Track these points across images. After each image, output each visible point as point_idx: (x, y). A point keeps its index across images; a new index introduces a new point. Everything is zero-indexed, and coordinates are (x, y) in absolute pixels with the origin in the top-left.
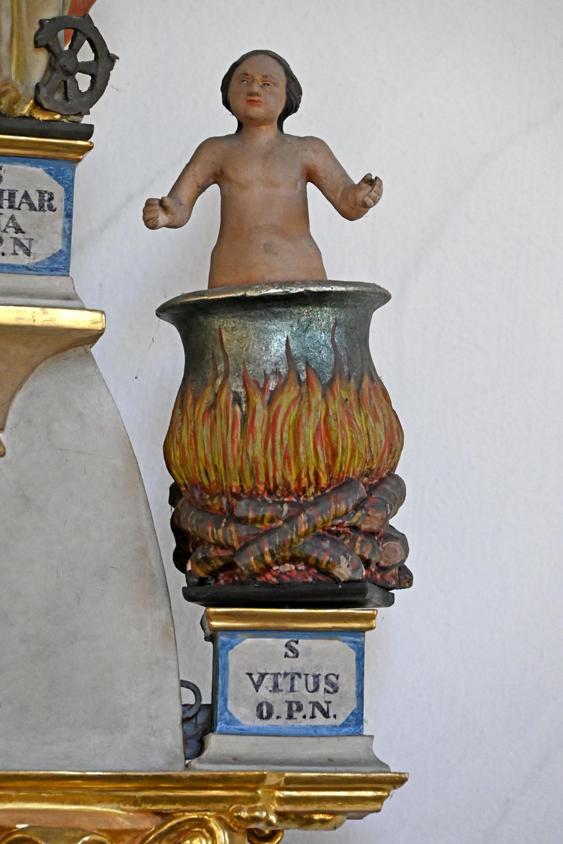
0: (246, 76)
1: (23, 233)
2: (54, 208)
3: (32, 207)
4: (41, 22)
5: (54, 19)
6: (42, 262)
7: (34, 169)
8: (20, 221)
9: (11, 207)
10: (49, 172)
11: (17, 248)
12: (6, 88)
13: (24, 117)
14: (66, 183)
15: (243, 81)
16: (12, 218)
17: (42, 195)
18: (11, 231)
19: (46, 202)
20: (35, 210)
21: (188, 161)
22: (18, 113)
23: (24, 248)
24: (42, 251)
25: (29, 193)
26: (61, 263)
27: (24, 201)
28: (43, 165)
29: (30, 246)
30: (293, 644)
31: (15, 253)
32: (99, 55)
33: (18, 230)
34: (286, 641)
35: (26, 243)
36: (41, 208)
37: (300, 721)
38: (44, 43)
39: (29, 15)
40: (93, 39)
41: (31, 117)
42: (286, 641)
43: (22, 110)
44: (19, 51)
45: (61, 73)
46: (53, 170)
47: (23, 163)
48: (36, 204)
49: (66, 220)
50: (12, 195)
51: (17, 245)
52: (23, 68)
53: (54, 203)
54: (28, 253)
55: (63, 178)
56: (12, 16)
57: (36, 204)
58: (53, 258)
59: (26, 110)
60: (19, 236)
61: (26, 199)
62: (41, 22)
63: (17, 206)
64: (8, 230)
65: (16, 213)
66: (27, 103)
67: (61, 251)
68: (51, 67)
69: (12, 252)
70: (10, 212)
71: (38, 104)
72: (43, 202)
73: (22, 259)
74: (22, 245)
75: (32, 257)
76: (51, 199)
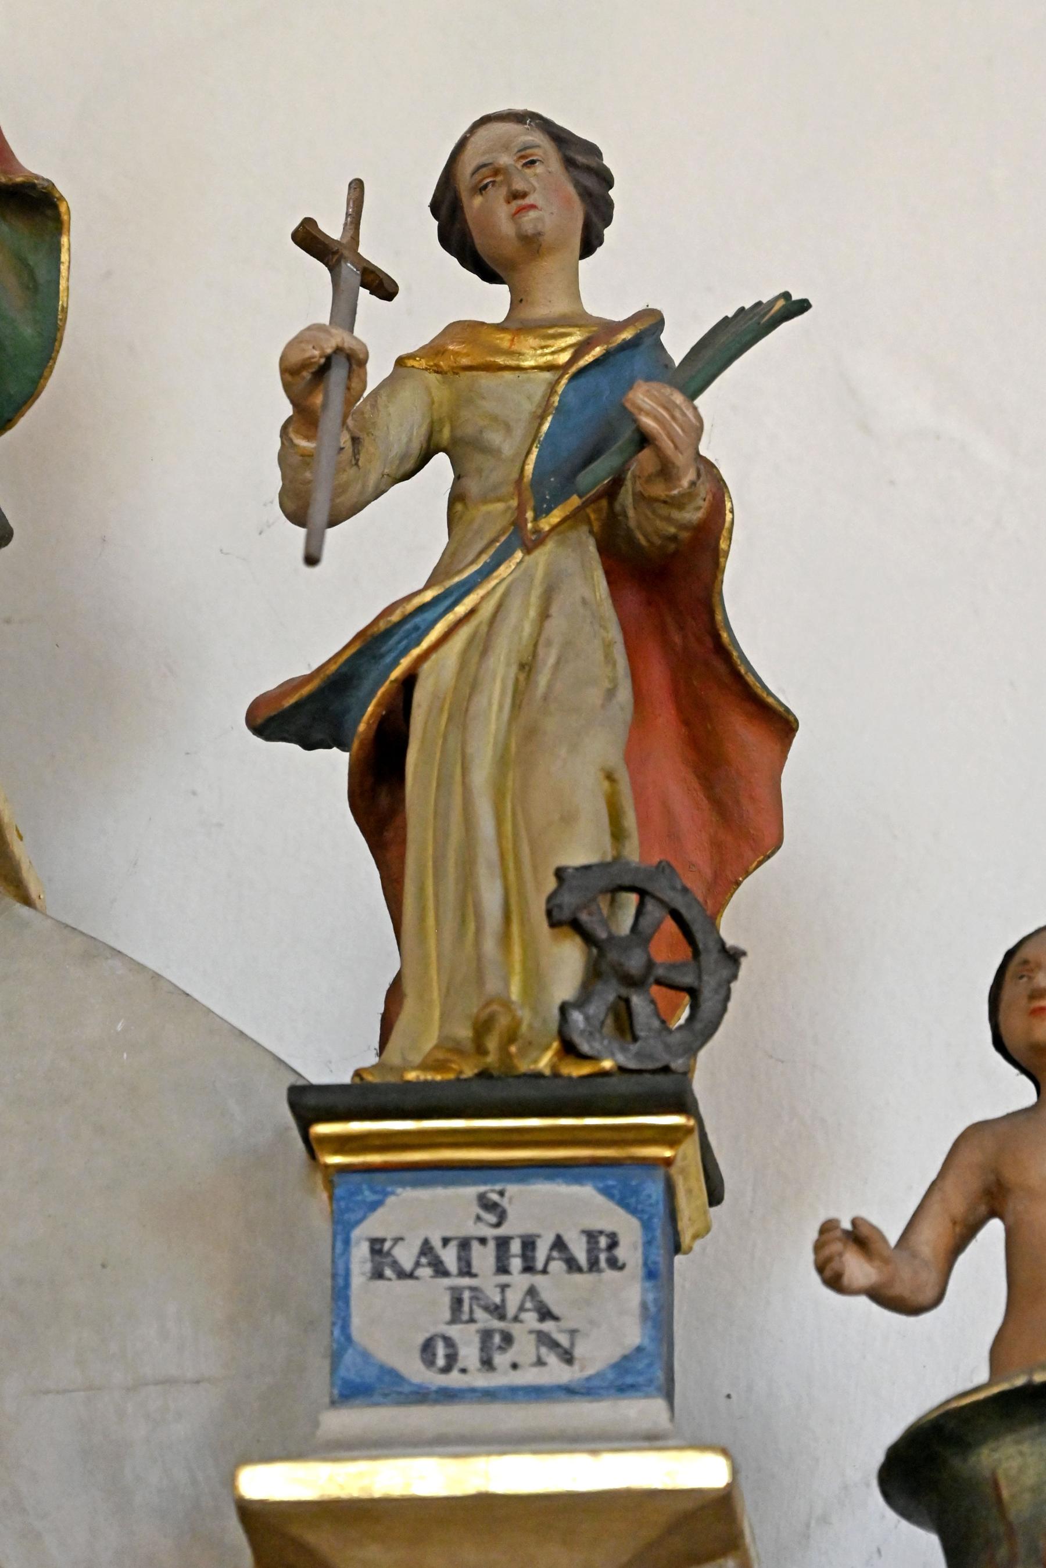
0: (1027, 967)
1: (556, 1318)
2: (620, 1264)
3: (572, 1266)
4: (560, 874)
5: (587, 868)
6: (600, 1375)
7: (575, 1189)
8: (549, 1296)
9: (528, 1269)
10: (607, 1192)
11: (544, 1350)
12: (488, 1011)
13: (538, 1076)
14: (643, 1211)
15: (1022, 977)
16: (532, 1292)
17: (592, 1240)
18: (530, 1318)
19: (603, 1251)
20: (580, 1270)
21: (933, 1175)
22: (524, 1066)
23: (560, 1350)
24: (596, 1354)
25: (566, 1238)
26: (640, 1373)
27: (555, 1254)
28: (593, 1178)
29: (572, 1344)
31: (540, 1362)
32: (701, 946)
33: (545, 1314)
35: (563, 1340)
36: (594, 1265)
38: (566, 915)
39: (535, 868)
40: (683, 911)
41: (556, 1075)
43: (536, 1061)
44: (525, 947)
45: (614, 982)
46: (613, 1187)
47: (550, 1178)
48: (582, 1258)
49: (648, 1284)
50: (529, 1244)
51: (544, 1344)
52: (535, 979)
53: (620, 1253)
54: (568, 1357)
55: (638, 1202)
56: (505, 877)
57: (582, 1258)
58: (624, 1365)
59: (544, 1062)
60: (548, 1326)
61: (560, 1251)
62: (560, 874)
63: (540, 1265)
64: (524, 1316)
65: (539, 1280)
66: (547, 1048)
67: (639, 1349)
68: (594, 974)
69: (534, 1359)
70: (527, 1280)
71: (569, 1049)
72: (595, 1252)
73: (556, 1372)
74: (554, 1345)
75: (576, 1367)
76: (613, 1245)
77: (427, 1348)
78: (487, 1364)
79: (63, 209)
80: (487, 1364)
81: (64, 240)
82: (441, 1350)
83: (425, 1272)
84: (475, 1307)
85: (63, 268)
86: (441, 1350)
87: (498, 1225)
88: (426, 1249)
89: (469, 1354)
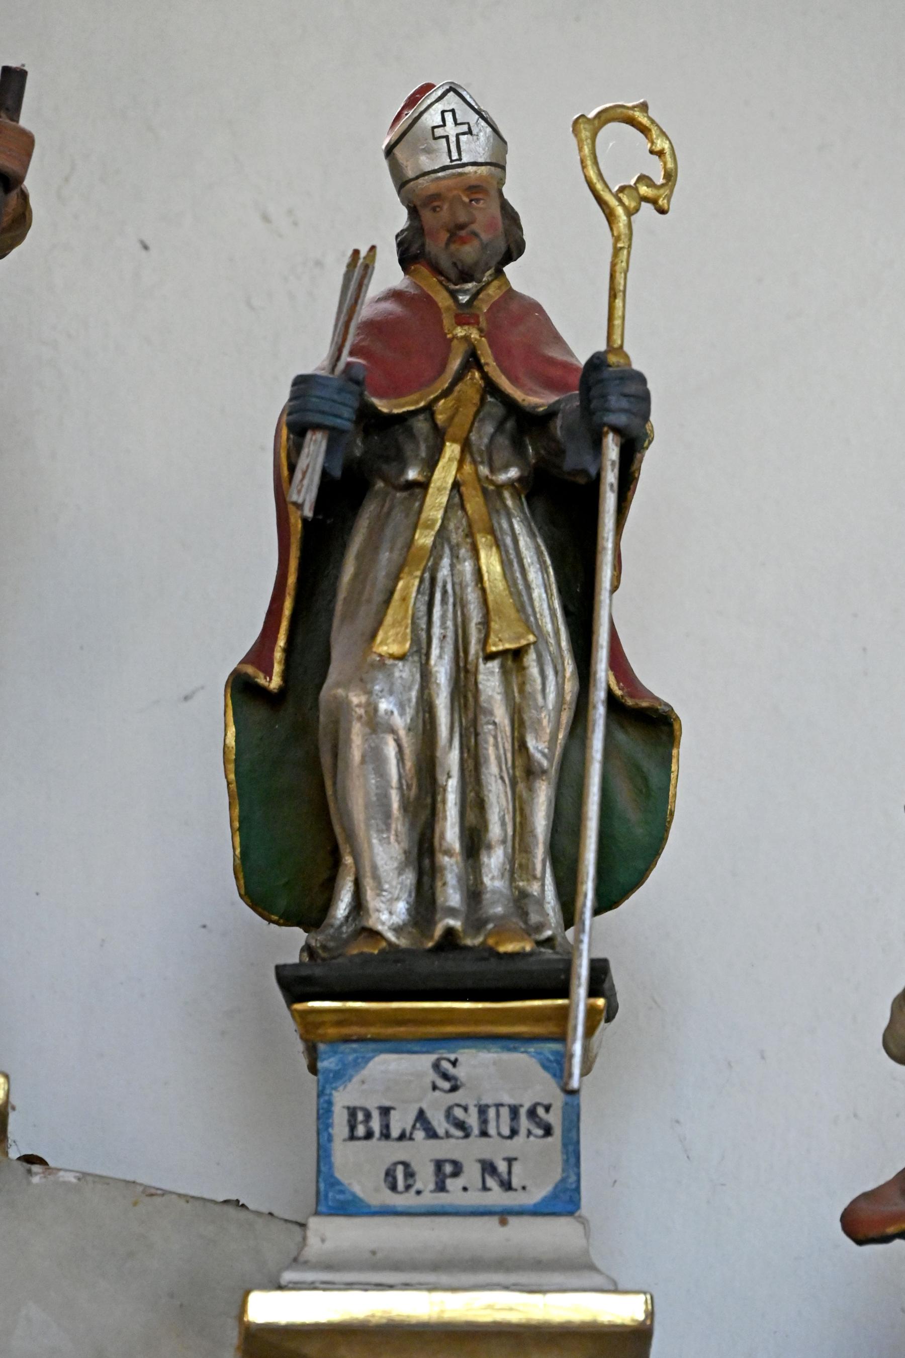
30: (445, 1065)
31: (485, 1188)
34: (433, 1057)
37: (455, 1194)
42: (433, 1057)
54: (507, 1186)
73: (497, 1197)
77: (390, 1174)
78: (441, 1187)
79: (676, 727)
80: (441, 1187)
81: (674, 752)
82: (400, 1172)
83: (419, 1135)
84: (418, 1125)
85: (673, 776)
86: (400, 1172)
87: (439, 1060)
88: (421, 1115)
89: (425, 1178)
